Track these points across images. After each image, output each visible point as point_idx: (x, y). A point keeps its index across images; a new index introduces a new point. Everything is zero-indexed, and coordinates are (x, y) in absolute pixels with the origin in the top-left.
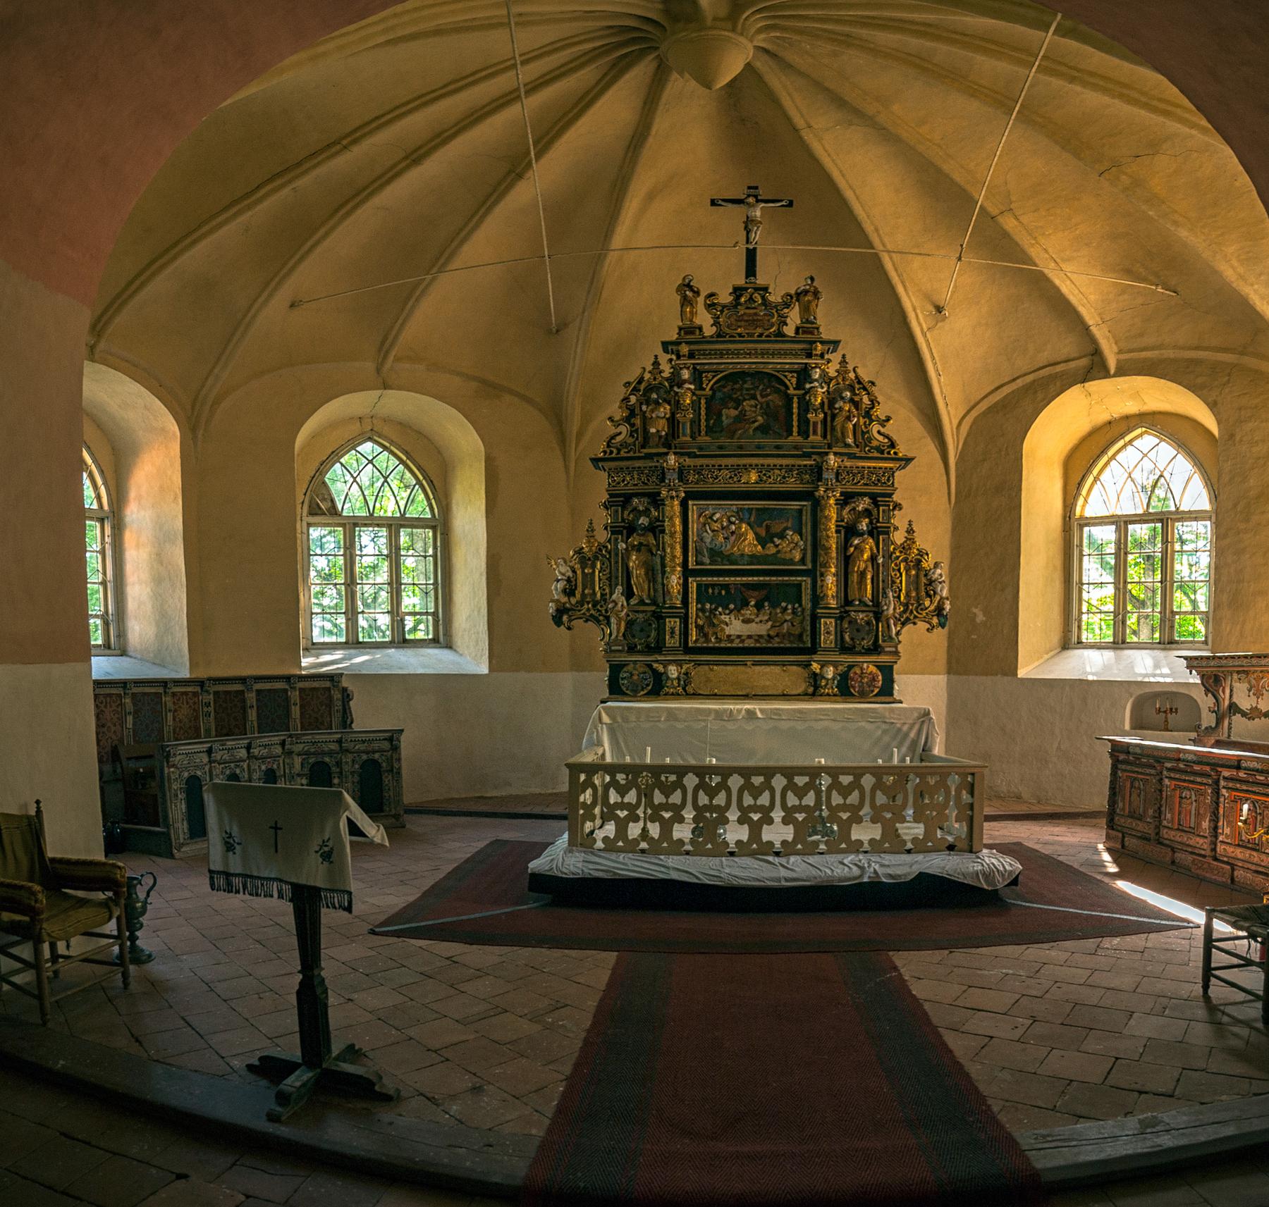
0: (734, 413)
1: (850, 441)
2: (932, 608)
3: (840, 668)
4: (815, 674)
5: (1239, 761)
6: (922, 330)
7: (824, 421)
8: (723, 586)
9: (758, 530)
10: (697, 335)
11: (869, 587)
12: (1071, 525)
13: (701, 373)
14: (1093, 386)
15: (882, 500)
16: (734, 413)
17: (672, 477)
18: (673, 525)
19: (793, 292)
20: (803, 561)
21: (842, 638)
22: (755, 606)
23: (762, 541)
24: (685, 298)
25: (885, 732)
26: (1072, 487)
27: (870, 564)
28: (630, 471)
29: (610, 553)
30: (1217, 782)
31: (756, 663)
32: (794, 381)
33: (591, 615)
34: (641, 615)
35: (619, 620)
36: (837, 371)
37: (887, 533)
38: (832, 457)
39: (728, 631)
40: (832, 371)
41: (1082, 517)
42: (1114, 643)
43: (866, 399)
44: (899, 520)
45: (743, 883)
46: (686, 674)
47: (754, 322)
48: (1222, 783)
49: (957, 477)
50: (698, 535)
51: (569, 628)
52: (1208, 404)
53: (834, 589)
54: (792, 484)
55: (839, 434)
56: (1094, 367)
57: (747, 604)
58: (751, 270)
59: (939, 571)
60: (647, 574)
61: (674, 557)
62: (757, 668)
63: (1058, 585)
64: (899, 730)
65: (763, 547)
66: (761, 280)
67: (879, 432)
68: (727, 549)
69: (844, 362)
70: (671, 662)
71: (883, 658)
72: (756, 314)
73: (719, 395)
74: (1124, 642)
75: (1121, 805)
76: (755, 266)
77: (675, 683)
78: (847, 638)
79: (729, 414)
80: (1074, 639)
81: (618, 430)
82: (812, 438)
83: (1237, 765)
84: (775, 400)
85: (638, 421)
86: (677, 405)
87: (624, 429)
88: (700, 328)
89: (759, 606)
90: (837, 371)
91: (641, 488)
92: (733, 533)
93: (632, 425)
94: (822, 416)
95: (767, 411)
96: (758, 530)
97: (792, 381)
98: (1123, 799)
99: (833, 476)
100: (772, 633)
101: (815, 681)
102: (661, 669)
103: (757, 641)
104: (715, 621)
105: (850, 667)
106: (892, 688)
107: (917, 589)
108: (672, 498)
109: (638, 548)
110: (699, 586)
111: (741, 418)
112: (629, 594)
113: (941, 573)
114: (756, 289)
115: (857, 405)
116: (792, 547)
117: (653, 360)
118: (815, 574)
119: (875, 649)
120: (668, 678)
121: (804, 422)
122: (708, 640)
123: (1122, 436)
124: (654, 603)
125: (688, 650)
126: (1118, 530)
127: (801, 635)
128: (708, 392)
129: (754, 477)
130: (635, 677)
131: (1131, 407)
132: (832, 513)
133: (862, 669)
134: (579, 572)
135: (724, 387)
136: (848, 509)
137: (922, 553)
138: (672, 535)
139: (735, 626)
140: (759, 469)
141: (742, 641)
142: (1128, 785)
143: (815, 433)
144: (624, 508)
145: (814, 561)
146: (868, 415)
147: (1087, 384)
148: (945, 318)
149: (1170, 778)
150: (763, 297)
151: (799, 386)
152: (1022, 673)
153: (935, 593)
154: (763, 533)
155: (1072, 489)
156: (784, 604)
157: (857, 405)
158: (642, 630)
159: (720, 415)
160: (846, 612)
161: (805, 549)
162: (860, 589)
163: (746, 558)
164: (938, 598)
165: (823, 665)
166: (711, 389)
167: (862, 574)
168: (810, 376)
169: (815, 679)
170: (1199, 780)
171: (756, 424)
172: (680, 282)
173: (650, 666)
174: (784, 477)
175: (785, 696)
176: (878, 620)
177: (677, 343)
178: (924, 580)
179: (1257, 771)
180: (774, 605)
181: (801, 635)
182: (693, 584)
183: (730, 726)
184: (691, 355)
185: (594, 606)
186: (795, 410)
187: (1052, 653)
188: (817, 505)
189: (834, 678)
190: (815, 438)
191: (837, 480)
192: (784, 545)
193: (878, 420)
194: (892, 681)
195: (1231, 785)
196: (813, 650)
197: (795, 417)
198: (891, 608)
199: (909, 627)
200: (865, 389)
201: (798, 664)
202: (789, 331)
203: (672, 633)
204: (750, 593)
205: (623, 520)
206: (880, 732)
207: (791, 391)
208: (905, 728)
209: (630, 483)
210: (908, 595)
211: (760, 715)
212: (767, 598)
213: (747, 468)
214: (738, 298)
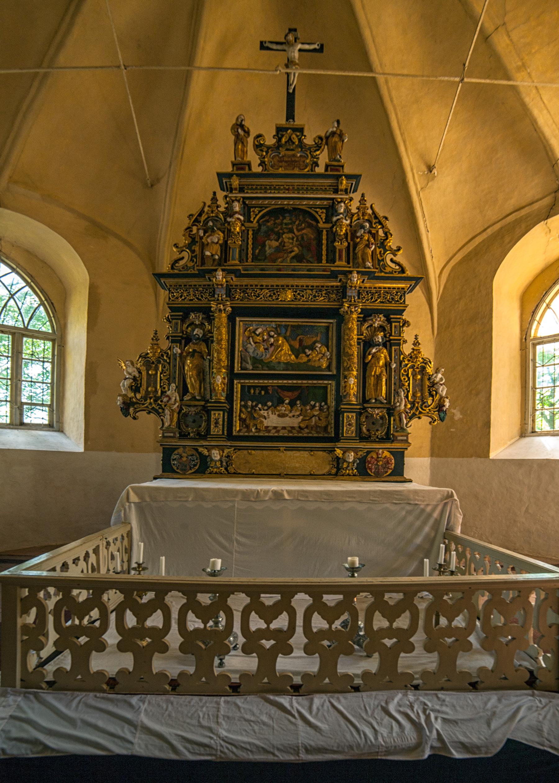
0: (275, 244)
1: (369, 264)
3: (360, 453)
4: (338, 458)
7: (348, 247)
8: (262, 386)
9: (292, 343)
10: (247, 171)
11: (384, 388)
13: (249, 208)
15: (394, 316)
16: (275, 244)
17: (221, 293)
18: (220, 334)
19: (323, 135)
20: (329, 368)
21: (360, 429)
22: (289, 404)
23: (296, 352)
24: (237, 136)
25: (409, 512)
26: (526, 325)
27: (384, 369)
28: (187, 288)
29: (170, 358)
31: (288, 449)
32: (323, 216)
33: (153, 408)
34: (193, 409)
35: (172, 411)
36: (358, 208)
37: (399, 345)
38: (355, 275)
39: (266, 423)
40: (354, 207)
43: (381, 233)
44: (408, 334)
45: (251, 757)
46: (228, 457)
47: (292, 163)
49: (438, 315)
50: (243, 346)
51: (134, 418)
53: (355, 389)
54: (321, 302)
55: (360, 260)
57: (283, 402)
58: (290, 115)
59: (440, 376)
60: (198, 375)
61: (220, 360)
62: (289, 453)
64: (423, 510)
65: (297, 357)
66: (298, 121)
68: (266, 357)
69: (363, 200)
70: (214, 447)
71: (396, 445)
72: (294, 156)
73: (264, 228)
76: (293, 111)
77: (218, 464)
78: (364, 429)
79: (272, 244)
80: (530, 429)
81: (181, 256)
82: (337, 263)
84: (308, 233)
85: (197, 248)
86: (229, 233)
87: (186, 255)
88: (249, 165)
89: (292, 404)
90: (358, 208)
91: (196, 303)
92: (272, 345)
93: (193, 252)
94: (346, 244)
95: (303, 243)
96: (292, 343)
97: (322, 215)
99: (355, 294)
100: (302, 425)
101: (338, 464)
102: (206, 452)
103: (290, 431)
104: (255, 415)
105: (368, 453)
107: (422, 391)
108: (220, 310)
109: (192, 354)
110: (243, 387)
111: (280, 249)
112: (183, 390)
114: (295, 130)
115: (374, 236)
116: (321, 357)
117: (211, 196)
118: (338, 377)
119: (388, 438)
120: (212, 460)
121: (332, 250)
122: (249, 430)
124: (203, 399)
125: (230, 437)
127: (326, 428)
128: (255, 224)
129: (289, 295)
130: (184, 459)
132: (354, 325)
133: (377, 454)
134: (144, 373)
135: (268, 221)
136: (366, 325)
137: (426, 362)
138: (219, 342)
139: (271, 420)
140: (295, 288)
141: (278, 431)
143: (340, 259)
144: (183, 321)
145: (338, 368)
146: (382, 245)
147: (549, 220)
150: (300, 140)
151: (328, 220)
152: (492, 455)
154: (297, 346)
156: (312, 403)
157: (374, 236)
158: (194, 421)
159: (264, 245)
160: (364, 408)
161: (331, 359)
162: (376, 390)
163: (282, 365)
165: (345, 451)
166: (258, 222)
167: (378, 378)
168: (336, 211)
169: (338, 462)
171: (293, 254)
172: (234, 122)
173: (197, 450)
174: (315, 296)
175: (312, 476)
176: (390, 415)
177: (229, 176)
180: (304, 404)
181: (326, 428)
182: (237, 386)
183: (257, 506)
184: (241, 190)
185: (155, 401)
186: (324, 242)
188: (341, 320)
189: (354, 462)
190: (341, 264)
191: (359, 298)
192: (314, 355)
193: (391, 249)
196: (337, 438)
197: (324, 248)
198: (402, 405)
199: (415, 421)
200: (380, 223)
201: (324, 450)
202: (320, 170)
203: (217, 423)
204: (286, 393)
205: (182, 332)
206: (404, 513)
207: (321, 225)
208: (429, 509)
209: (187, 299)
210: (414, 395)
211: (287, 496)
212: (299, 398)
213: (284, 288)
214: (280, 140)
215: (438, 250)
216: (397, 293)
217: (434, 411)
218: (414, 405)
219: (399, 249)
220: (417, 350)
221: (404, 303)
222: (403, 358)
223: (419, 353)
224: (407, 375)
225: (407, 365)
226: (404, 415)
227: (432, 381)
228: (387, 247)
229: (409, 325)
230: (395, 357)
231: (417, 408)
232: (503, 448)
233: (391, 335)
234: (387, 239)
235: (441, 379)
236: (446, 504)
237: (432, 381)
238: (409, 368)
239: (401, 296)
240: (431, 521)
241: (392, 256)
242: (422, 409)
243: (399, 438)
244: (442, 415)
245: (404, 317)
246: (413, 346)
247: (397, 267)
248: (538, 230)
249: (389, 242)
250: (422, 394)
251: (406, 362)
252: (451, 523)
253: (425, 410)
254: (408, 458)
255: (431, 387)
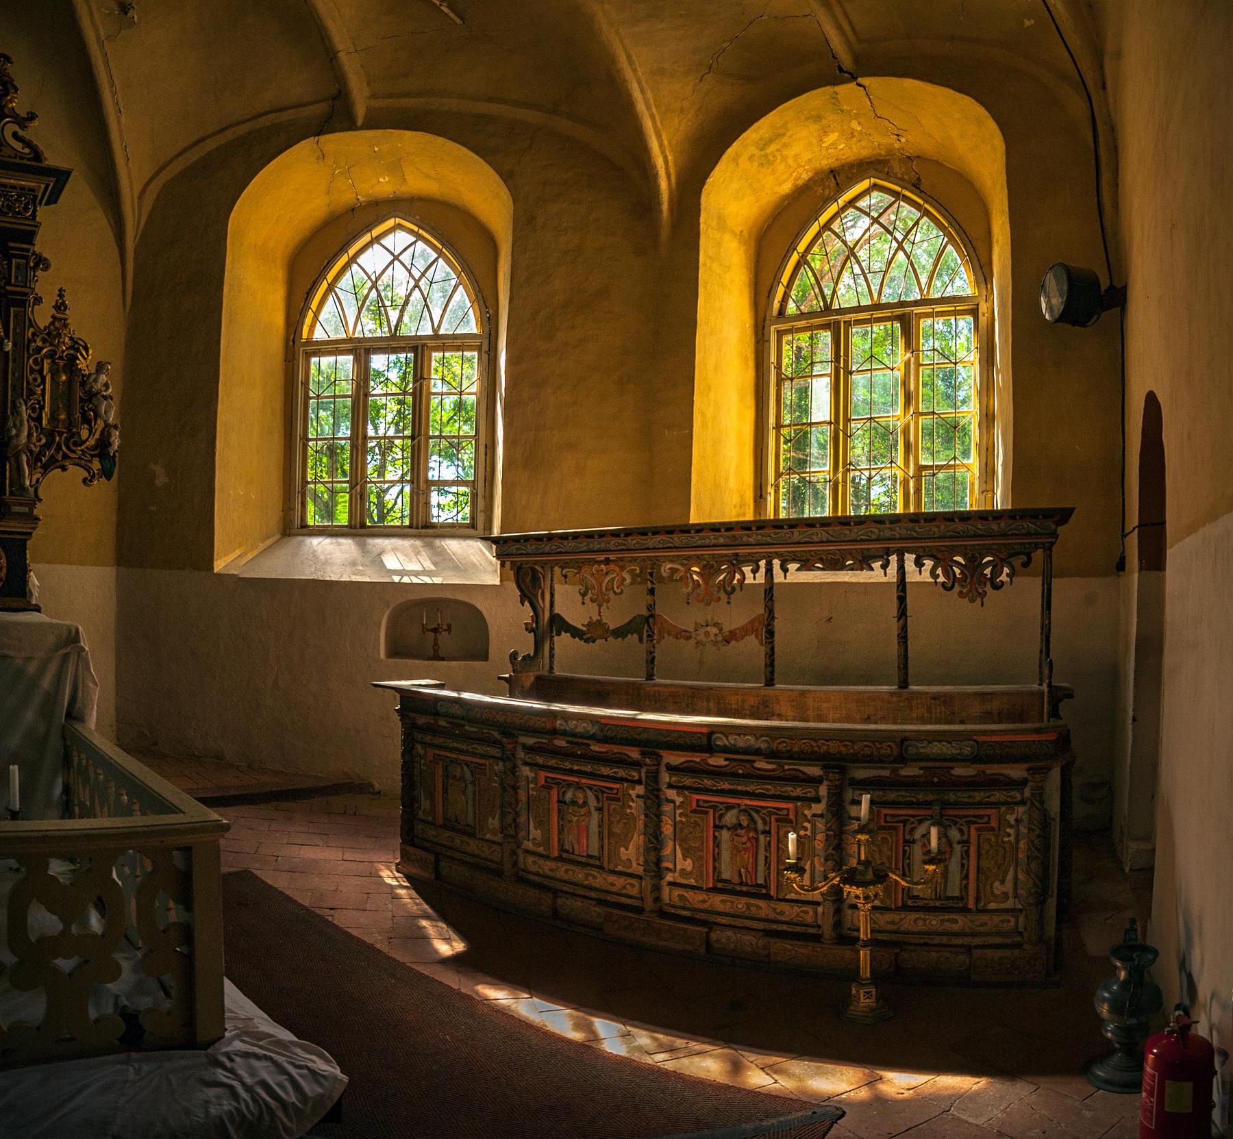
2: (91, 442)
5: (710, 734)
6: (98, 37)
12: (296, 350)
14: (332, 141)
30: (654, 777)
37: (23, 304)
41: (309, 342)
42: (350, 526)
44: (45, 285)
48: (665, 777)
52: (501, 174)
56: (335, 115)
59: (103, 378)
63: (277, 441)
67: (15, 135)
74: (363, 526)
75: (426, 804)
80: (297, 522)
83: (705, 741)
98: (432, 798)
106: (24, 581)
107: (69, 408)
113: (108, 383)
123: (368, 228)
126: (357, 360)
131: (384, 185)
137: (76, 345)
142: (439, 771)
147: (323, 138)
148: (131, 24)
149: (680, 788)
152: (219, 565)
153: (97, 416)
155: (298, 304)
164: (100, 425)
170: (605, 771)
178: (79, 393)
179: (758, 752)
187: (269, 542)
194: (25, 570)
195: (688, 781)
208: (32, 668)
210: (53, 418)
215: (140, 150)
216: (19, 196)
217: (93, 456)
218: (54, 438)
219: (32, 117)
220: (60, 319)
221: (34, 219)
222: (33, 334)
223: (66, 326)
224: (41, 371)
225: (40, 349)
226: (24, 458)
227: (87, 388)
228: (6, 110)
229: (47, 268)
230: (15, 329)
231: (59, 444)
232: (238, 552)
233: (9, 283)
234: (7, 95)
235: (106, 385)
236: (66, 655)
237: (87, 388)
238: (46, 356)
239: (27, 204)
240: (36, 701)
241: (16, 128)
242: (68, 448)
243: (16, 509)
244: (107, 464)
245: (37, 249)
246: (54, 312)
247: (27, 150)
248: (305, 148)
249: (11, 101)
250: (69, 416)
251: (40, 344)
252: (78, 705)
253: (74, 452)
254: (43, 567)
255: (86, 401)
